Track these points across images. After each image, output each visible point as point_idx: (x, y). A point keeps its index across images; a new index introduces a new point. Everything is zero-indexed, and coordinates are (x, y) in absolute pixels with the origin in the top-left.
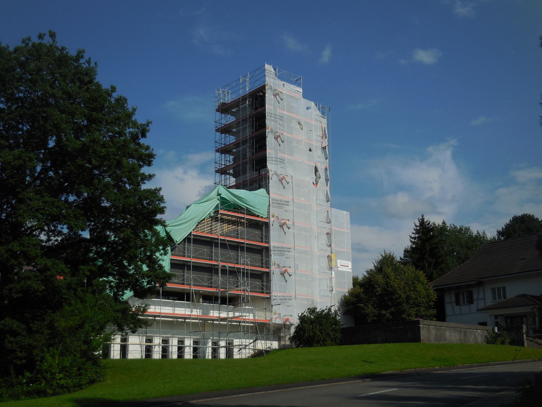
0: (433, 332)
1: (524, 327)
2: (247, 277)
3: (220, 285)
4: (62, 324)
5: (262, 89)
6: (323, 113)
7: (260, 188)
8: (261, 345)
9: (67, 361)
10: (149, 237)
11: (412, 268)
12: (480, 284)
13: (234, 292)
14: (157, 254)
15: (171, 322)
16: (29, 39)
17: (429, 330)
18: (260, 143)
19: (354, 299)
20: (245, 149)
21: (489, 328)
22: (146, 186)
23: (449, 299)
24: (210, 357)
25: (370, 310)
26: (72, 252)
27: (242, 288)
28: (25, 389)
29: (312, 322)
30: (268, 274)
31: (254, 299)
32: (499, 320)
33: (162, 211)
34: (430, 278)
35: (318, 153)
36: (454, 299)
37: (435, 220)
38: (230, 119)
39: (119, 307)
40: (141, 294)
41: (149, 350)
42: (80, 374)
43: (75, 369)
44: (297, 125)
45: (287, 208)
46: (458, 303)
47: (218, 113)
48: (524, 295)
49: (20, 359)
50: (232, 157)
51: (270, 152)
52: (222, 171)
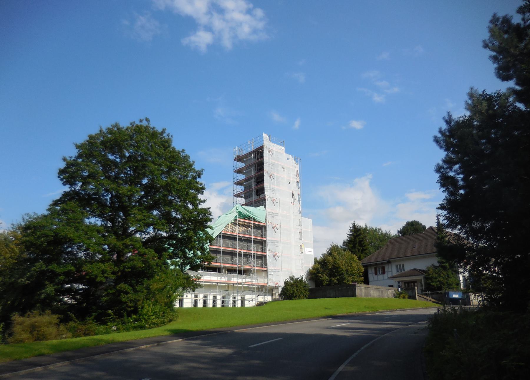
0: (363, 291)
1: (416, 288)
2: (254, 258)
3: (238, 263)
4: (155, 286)
5: (262, 148)
6: (296, 162)
7: (260, 206)
8: (262, 299)
9: (157, 308)
10: (202, 235)
11: (349, 253)
12: (389, 262)
13: (246, 267)
14: (206, 245)
15: (209, 285)
16: (134, 123)
17: (361, 289)
18: (260, 179)
19: (315, 271)
20: (252, 182)
21: (395, 288)
22: (202, 206)
23: (371, 271)
24: (232, 306)
25: (325, 278)
26: (155, 243)
27: (251, 265)
28: (133, 325)
29: (292, 285)
30: (265, 256)
31: (258, 270)
32: (401, 284)
33: (210, 220)
34: (359, 258)
35: (294, 185)
36: (373, 271)
37: (361, 224)
38: (242, 165)
39: (184, 276)
40: (195, 268)
41: (196, 302)
42: (164, 316)
43: (161, 313)
44: (281, 170)
45: (276, 217)
46: (376, 274)
47: (236, 162)
48: (415, 269)
49: (130, 307)
50: (243, 187)
51: (266, 185)
52: (238, 196)
